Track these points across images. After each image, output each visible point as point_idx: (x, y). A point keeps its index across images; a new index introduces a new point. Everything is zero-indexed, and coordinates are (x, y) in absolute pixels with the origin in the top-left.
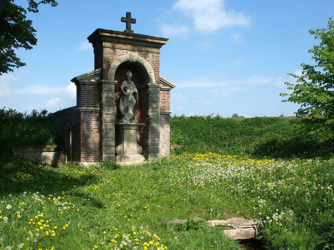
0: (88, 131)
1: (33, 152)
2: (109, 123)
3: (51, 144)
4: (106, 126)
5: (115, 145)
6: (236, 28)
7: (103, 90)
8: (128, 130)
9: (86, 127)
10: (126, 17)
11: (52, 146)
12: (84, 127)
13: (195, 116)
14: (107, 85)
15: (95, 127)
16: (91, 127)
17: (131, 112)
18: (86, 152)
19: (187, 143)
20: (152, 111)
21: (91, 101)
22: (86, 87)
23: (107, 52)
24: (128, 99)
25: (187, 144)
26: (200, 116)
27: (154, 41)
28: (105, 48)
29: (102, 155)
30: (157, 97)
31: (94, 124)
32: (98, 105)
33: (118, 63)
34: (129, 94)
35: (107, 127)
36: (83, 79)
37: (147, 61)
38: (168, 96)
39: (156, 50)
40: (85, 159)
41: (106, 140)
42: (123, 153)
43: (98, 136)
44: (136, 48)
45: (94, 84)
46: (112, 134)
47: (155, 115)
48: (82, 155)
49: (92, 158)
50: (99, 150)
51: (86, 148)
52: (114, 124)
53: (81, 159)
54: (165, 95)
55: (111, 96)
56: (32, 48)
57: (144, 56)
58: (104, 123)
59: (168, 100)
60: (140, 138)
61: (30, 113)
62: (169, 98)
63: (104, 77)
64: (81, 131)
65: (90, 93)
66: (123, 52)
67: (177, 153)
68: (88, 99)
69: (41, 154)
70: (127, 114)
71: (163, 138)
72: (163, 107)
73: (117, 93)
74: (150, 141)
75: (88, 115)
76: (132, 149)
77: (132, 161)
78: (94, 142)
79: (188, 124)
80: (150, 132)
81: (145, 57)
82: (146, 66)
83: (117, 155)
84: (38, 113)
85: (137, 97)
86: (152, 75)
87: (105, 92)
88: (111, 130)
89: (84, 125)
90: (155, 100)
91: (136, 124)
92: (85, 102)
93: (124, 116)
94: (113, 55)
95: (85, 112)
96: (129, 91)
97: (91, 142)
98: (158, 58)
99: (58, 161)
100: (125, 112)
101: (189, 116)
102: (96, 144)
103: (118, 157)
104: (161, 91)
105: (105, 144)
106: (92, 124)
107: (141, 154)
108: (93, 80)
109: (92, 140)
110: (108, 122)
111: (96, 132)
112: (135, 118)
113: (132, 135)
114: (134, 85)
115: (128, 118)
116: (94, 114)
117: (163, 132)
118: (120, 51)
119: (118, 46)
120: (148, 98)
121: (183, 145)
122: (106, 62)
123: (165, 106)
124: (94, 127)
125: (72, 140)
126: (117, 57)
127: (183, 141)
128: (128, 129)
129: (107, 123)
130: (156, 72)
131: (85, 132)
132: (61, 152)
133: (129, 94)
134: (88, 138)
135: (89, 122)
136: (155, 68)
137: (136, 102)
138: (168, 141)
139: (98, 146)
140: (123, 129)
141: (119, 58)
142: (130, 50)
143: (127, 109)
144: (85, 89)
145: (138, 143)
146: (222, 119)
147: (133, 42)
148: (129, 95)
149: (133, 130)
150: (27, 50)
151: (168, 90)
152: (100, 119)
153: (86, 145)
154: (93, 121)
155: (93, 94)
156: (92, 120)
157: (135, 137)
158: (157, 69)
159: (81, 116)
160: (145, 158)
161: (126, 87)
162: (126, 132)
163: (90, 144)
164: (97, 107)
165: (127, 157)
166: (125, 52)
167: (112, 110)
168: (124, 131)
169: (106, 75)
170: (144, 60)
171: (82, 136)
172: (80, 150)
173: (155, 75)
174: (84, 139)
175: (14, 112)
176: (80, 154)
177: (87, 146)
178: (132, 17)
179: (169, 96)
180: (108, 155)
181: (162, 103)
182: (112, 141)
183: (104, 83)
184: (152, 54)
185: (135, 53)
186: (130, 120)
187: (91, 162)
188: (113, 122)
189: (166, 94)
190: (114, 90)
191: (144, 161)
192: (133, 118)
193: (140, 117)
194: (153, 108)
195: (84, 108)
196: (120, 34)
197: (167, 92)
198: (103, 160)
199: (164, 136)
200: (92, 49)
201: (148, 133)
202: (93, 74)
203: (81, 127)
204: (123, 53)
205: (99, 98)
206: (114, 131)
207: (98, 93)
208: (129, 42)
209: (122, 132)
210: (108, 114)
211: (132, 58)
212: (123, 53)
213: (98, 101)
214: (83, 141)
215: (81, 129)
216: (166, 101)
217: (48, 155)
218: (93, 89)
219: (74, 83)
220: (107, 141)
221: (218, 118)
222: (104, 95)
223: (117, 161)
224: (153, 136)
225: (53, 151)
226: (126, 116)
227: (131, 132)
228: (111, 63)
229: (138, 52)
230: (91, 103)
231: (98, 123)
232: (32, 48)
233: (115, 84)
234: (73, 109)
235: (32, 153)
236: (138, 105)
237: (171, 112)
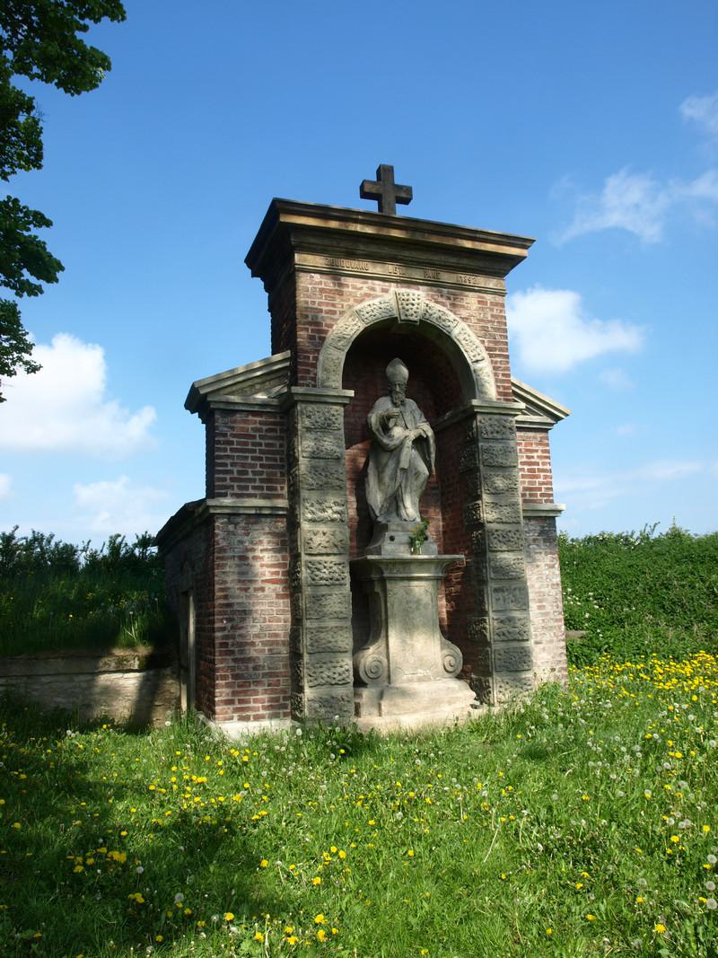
0: (243, 594)
1: (64, 674)
2: (328, 555)
3: (131, 645)
4: (313, 568)
5: (355, 640)
6: (612, 359)
7: (299, 427)
8: (405, 583)
9: (236, 577)
10: (375, 179)
11: (135, 651)
12: (227, 576)
13: (601, 535)
14: (314, 406)
15: (273, 573)
16: (256, 575)
17: (410, 508)
18: (235, 677)
19: (596, 623)
20: (495, 505)
21: (255, 473)
22: (235, 422)
23: (310, 286)
24: (398, 462)
25: (600, 625)
26: (615, 534)
27: (482, 248)
28: (301, 274)
29: (301, 690)
30: (508, 451)
31: (266, 561)
32: (282, 488)
33: (356, 327)
34: (402, 444)
35: (317, 573)
36: (222, 392)
37: (463, 319)
38: (543, 451)
39: (492, 283)
40: (231, 707)
41: (315, 625)
42: (389, 677)
43: (284, 612)
44: (417, 274)
45: (268, 410)
46: (339, 601)
47: (504, 520)
48: (221, 693)
49: (260, 699)
50: (289, 670)
51: (235, 660)
52: (345, 559)
53: (218, 708)
54: (534, 447)
55: (328, 448)
56: (42, 292)
57: (448, 302)
58: (304, 558)
59: (544, 464)
60: (448, 612)
61: (101, 547)
62: (549, 458)
63: (303, 378)
64: (218, 594)
65: (253, 444)
66: (373, 289)
67: (574, 659)
68: (243, 465)
69: (93, 680)
70: (398, 520)
71: (540, 607)
72: (531, 489)
73: (354, 447)
74: (492, 623)
75: (244, 528)
76: (421, 659)
77: (426, 708)
78: (270, 635)
79: (584, 560)
80: (492, 585)
81: (453, 305)
82: (461, 337)
83: (364, 685)
84: (126, 545)
85: (433, 456)
86: (485, 370)
87: (308, 435)
88: (334, 583)
89: (228, 569)
90: (500, 460)
91: (433, 556)
92: (232, 479)
93: (385, 528)
94: (334, 299)
95: (233, 516)
96: (398, 432)
97: (257, 636)
98: (501, 311)
99: (157, 703)
100: (388, 512)
101: (582, 537)
102: (277, 643)
103: (366, 694)
104: (518, 434)
105: (312, 645)
106: (262, 566)
107: (459, 677)
108: (261, 397)
109: (262, 629)
110: (324, 551)
111: (278, 596)
112: (428, 533)
113: (418, 601)
114: (418, 413)
115: (402, 537)
116: (266, 526)
117: (537, 585)
118: (359, 285)
119: (348, 265)
120: (473, 455)
121: (588, 629)
122: (310, 323)
123: (537, 486)
124: (268, 577)
125: (197, 630)
126: (350, 307)
127: (587, 615)
128: (402, 579)
129: (319, 558)
130: (499, 359)
131: (233, 597)
132: (168, 671)
133: (402, 444)
134: (243, 620)
135: (250, 555)
136: (492, 345)
137: (427, 473)
138: (557, 620)
139: (284, 651)
140: (383, 581)
141: (358, 307)
142: (396, 282)
143: (395, 502)
144: (233, 428)
145: (443, 632)
146: (699, 542)
147: (407, 253)
148: (401, 445)
149: (423, 583)
150: (21, 296)
151: (543, 429)
152: (289, 543)
153: (237, 649)
154: (266, 550)
155: (263, 448)
156: (260, 547)
157: (430, 611)
158: (501, 350)
159: (217, 535)
160: (474, 694)
161: (389, 417)
162: (396, 591)
163: (253, 644)
164: (279, 496)
165: (404, 693)
166: (378, 288)
167: (334, 503)
168: (389, 586)
169: (308, 372)
170: (451, 316)
171: (220, 613)
172: (214, 670)
173: (494, 368)
174: (230, 625)
175: (49, 542)
176: (214, 686)
177: (242, 652)
178: (398, 180)
179: (548, 451)
180: (323, 691)
181: (523, 476)
182: (341, 628)
183: (303, 402)
184: (479, 297)
185: (416, 292)
186: (411, 543)
187: (257, 718)
188: (340, 554)
189: (538, 444)
190: (342, 426)
191: (475, 707)
192: (422, 536)
193: (444, 532)
194: (496, 493)
195: (227, 501)
196: (356, 221)
197: (539, 435)
198: (306, 711)
199: (540, 601)
200: (264, 297)
201: (481, 593)
202: (259, 373)
203: (216, 579)
204: (372, 293)
205: (285, 464)
206: (348, 586)
207: (281, 446)
208: (394, 252)
209: (381, 595)
210: (322, 521)
211: (407, 307)
212: (372, 293)
213: (282, 474)
214: (226, 633)
215: (217, 587)
216: (536, 467)
217: (121, 682)
218: (264, 427)
219: (197, 414)
220: (320, 630)
221: (676, 536)
222: (305, 446)
223: (363, 711)
224: (501, 601)
225: (136, 667)
226: (392, 527)
227: (417, 590)
228: (326, 325)
229: (426, 288)
230: (257, 484)
231: (284, 558)
232: (42, 292)
233: (347, 401)
234: (194, 512)
235: (61, 678)
236: (434, 488)
237: (559, 508)
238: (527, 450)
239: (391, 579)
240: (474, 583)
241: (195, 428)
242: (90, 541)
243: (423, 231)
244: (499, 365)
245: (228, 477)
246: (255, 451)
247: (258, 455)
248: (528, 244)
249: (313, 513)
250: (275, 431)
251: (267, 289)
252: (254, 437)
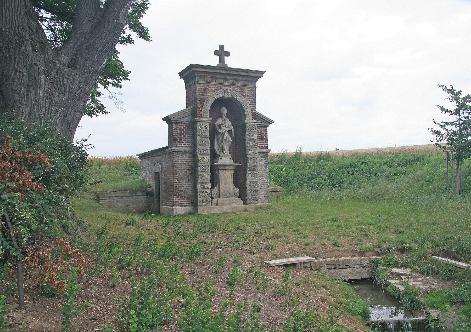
36: (175, 118)
54: (263, 132)
65: (183, 132)
68: (181, 138)
85: (233, 135)
93: (219, 156)
136: (251, 103)
140: (218, 170)
147: (227, 77)
174: (178, 181)
178: (226, 50)
190: (209, 128)
207: (191, 132)
214: (177, 183)
233: (210, 121)
238: (261, 133)
239: (221, 170)
240: (244, 171)
241: (165, 125)
242: (442, 108)
243: (233, 71)
244: (253, 109)
245: (177, 141)
246: (184, 134)
247: (184, 135)
248: (259, 75)
249: (201, 152)
250: (189, 128)
251: (185, 82)
252: (184, 130)
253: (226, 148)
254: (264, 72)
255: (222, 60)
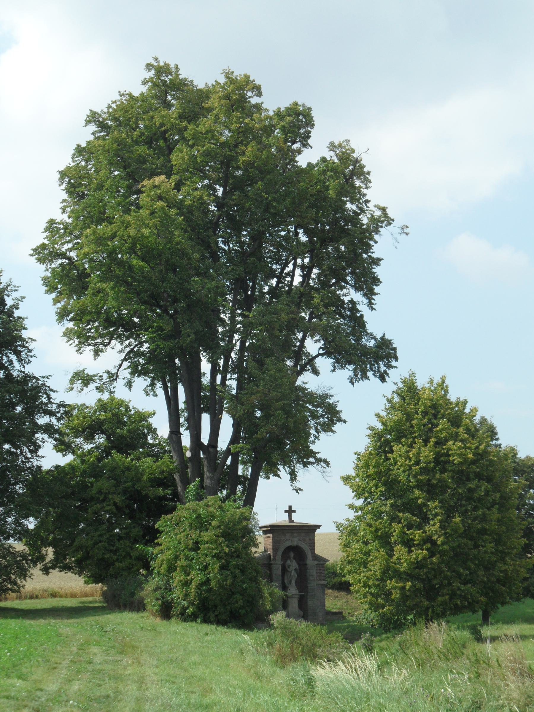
178: (287, 509)
253: (293, 582)
254: (320, 526)
255: (290, 517)
